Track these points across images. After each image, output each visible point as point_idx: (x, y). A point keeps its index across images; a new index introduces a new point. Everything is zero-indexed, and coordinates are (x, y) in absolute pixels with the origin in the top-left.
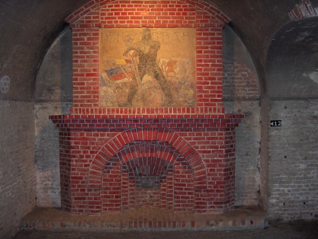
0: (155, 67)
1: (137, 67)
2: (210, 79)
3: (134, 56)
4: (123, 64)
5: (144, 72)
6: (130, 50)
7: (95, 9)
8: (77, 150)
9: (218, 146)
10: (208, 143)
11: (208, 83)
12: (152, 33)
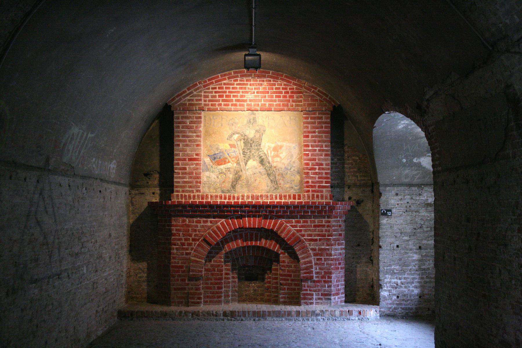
0: (260, 152)
1: (241, 152)
2: (317, 164)
3: (238, 141)
4: (227, 149)
5: (249, 157)
6: (234, 134)
7: (198, 91)
8: (178, 237)
9: (326, 234)
10: (315, 231)
11: (315, 169)
12: (257, 117)
